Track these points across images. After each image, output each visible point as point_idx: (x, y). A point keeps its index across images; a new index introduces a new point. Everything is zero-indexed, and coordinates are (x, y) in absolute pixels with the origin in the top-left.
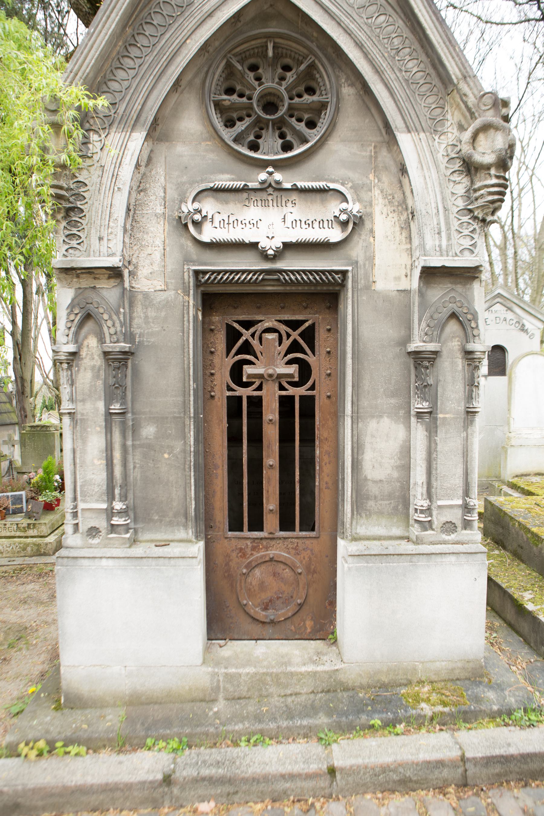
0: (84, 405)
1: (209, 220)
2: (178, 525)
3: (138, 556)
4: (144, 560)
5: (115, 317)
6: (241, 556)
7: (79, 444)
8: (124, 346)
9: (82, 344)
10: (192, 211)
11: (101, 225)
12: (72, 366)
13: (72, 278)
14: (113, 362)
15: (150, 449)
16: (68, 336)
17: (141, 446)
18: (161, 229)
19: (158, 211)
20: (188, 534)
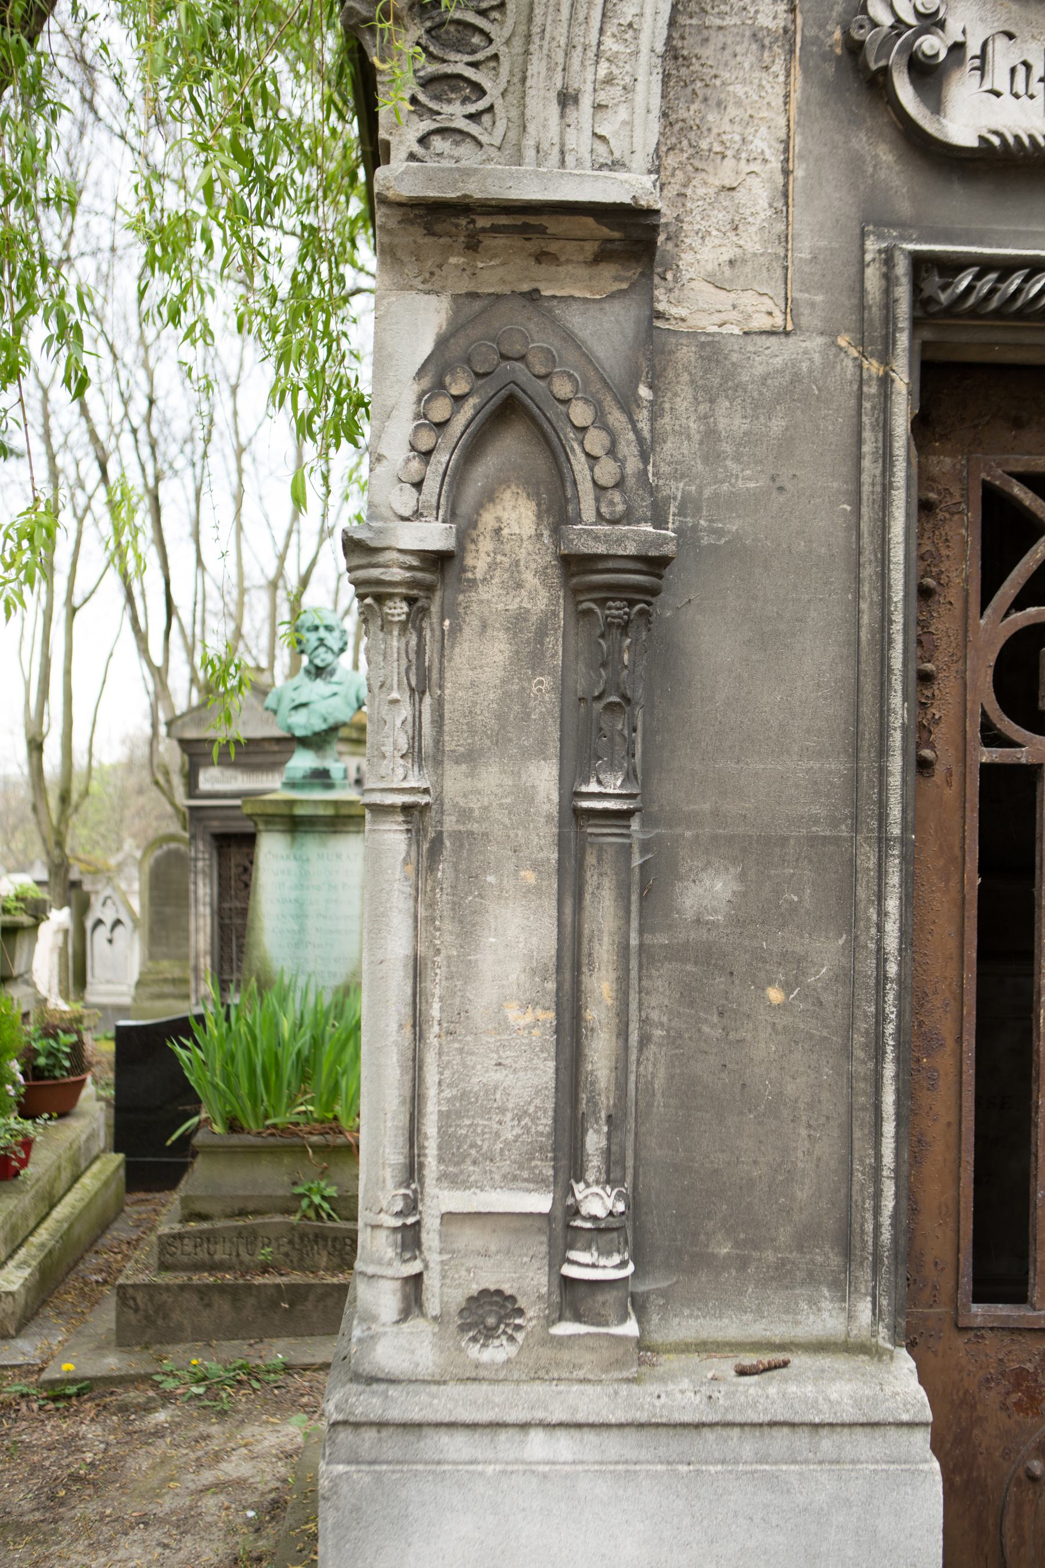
0: (471, 775)
1: (969, 64)
2: (812, 1279)
3: (687, 1418)
4: (709, 1434)
5: (616, 418)
6: (1018, 1404)
7: (447, 937)
8: (638, 536)
9: (474, 525)
10: (910, 19)
11: (570, 47)
12: (425, 611)
13: (447, 251)
14: (602, 602)
15: (709, 968)
16: (418, 485)
17: (677, 953)
18: (775, 94)
19: (765, 21)
20: (850, 1317)
